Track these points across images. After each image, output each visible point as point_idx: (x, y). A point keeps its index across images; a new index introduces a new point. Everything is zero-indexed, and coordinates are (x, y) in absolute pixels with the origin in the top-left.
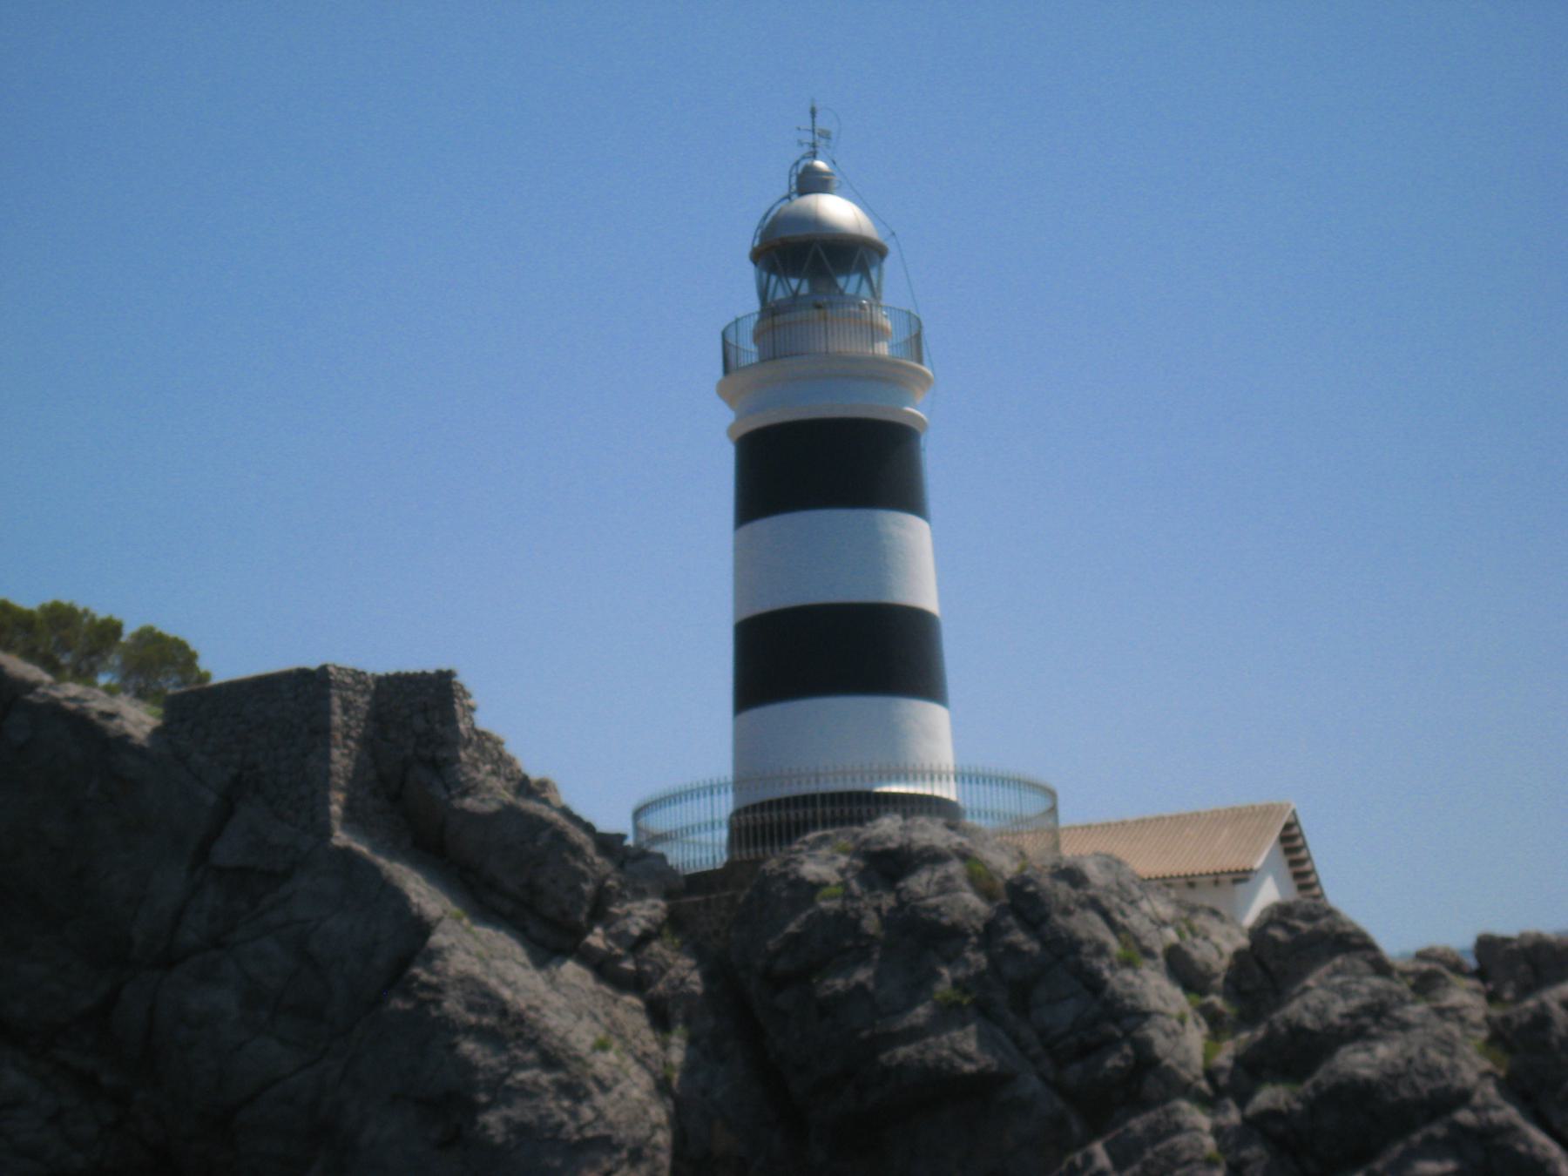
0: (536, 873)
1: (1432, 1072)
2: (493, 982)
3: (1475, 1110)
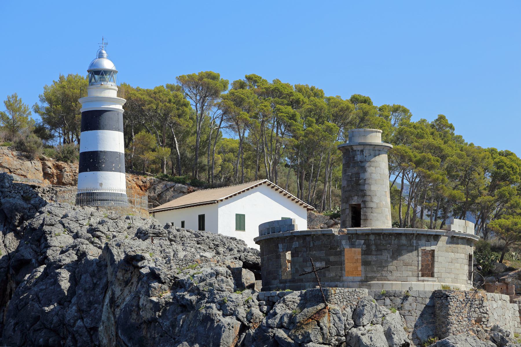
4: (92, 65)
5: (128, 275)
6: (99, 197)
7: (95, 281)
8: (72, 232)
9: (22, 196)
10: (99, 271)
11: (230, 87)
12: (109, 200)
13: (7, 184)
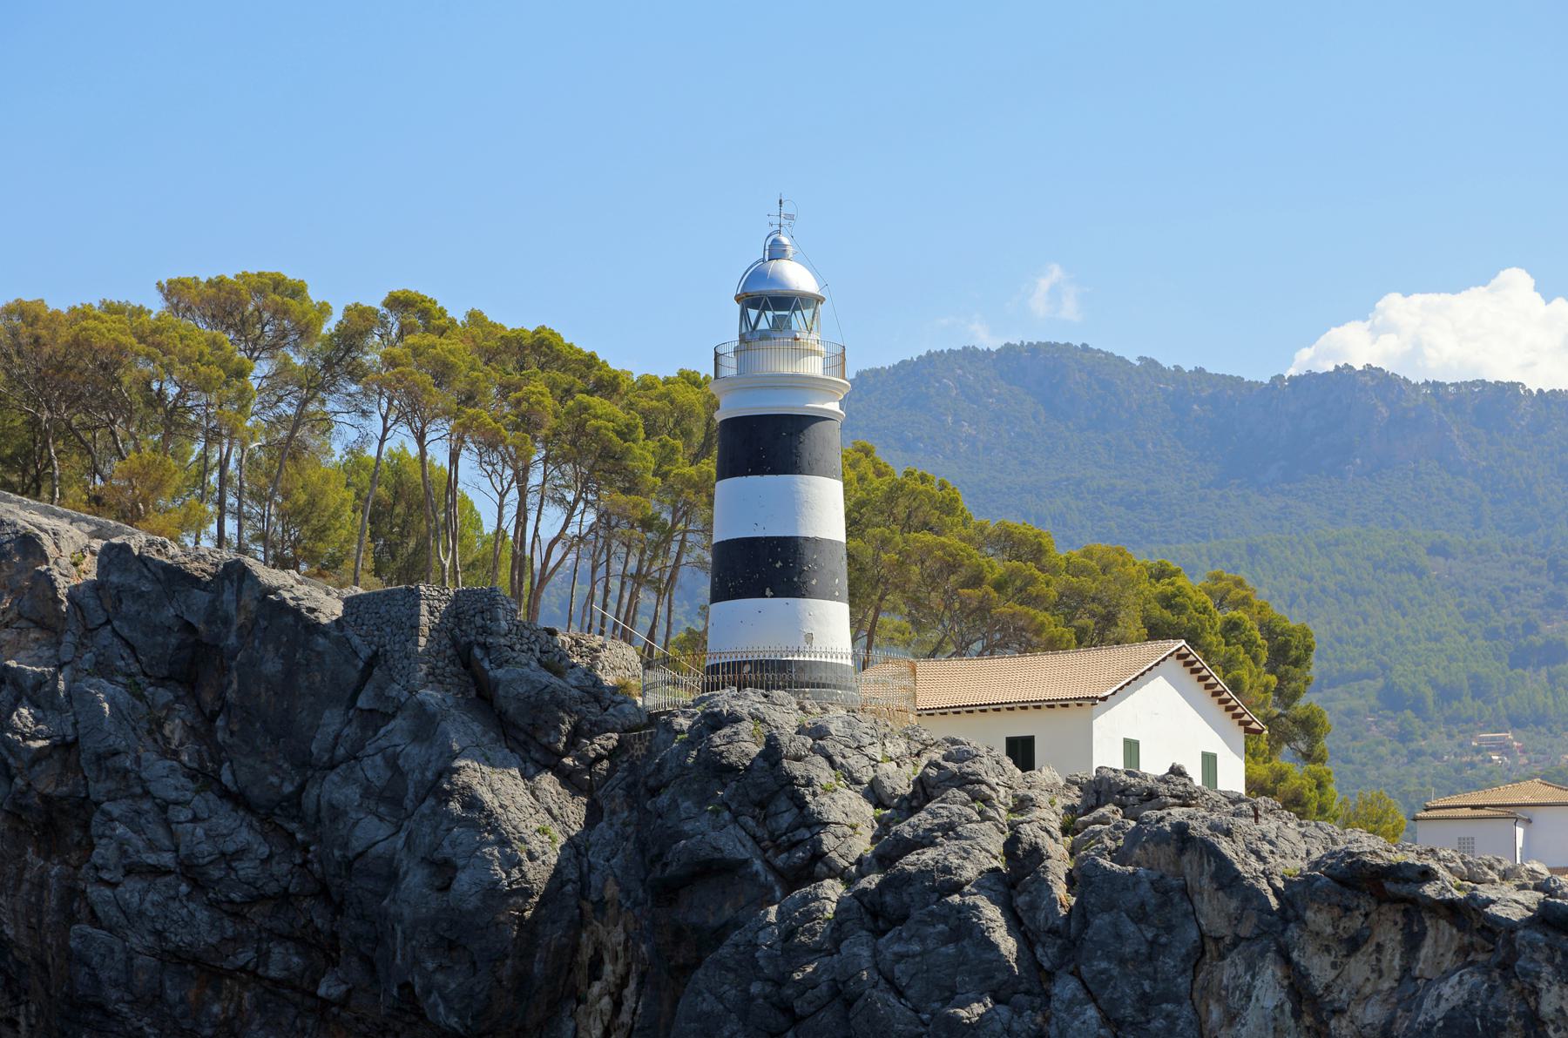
1: (947, 870)
4: (757, 275)
5: (1355, 922)
6: (805, 678)
7: (1149, 936)
8: (859, 783)
9: (539, 660)
10: (1162, 906)
11: (153, 316)
12: (829, 686)
13: (503, 623)
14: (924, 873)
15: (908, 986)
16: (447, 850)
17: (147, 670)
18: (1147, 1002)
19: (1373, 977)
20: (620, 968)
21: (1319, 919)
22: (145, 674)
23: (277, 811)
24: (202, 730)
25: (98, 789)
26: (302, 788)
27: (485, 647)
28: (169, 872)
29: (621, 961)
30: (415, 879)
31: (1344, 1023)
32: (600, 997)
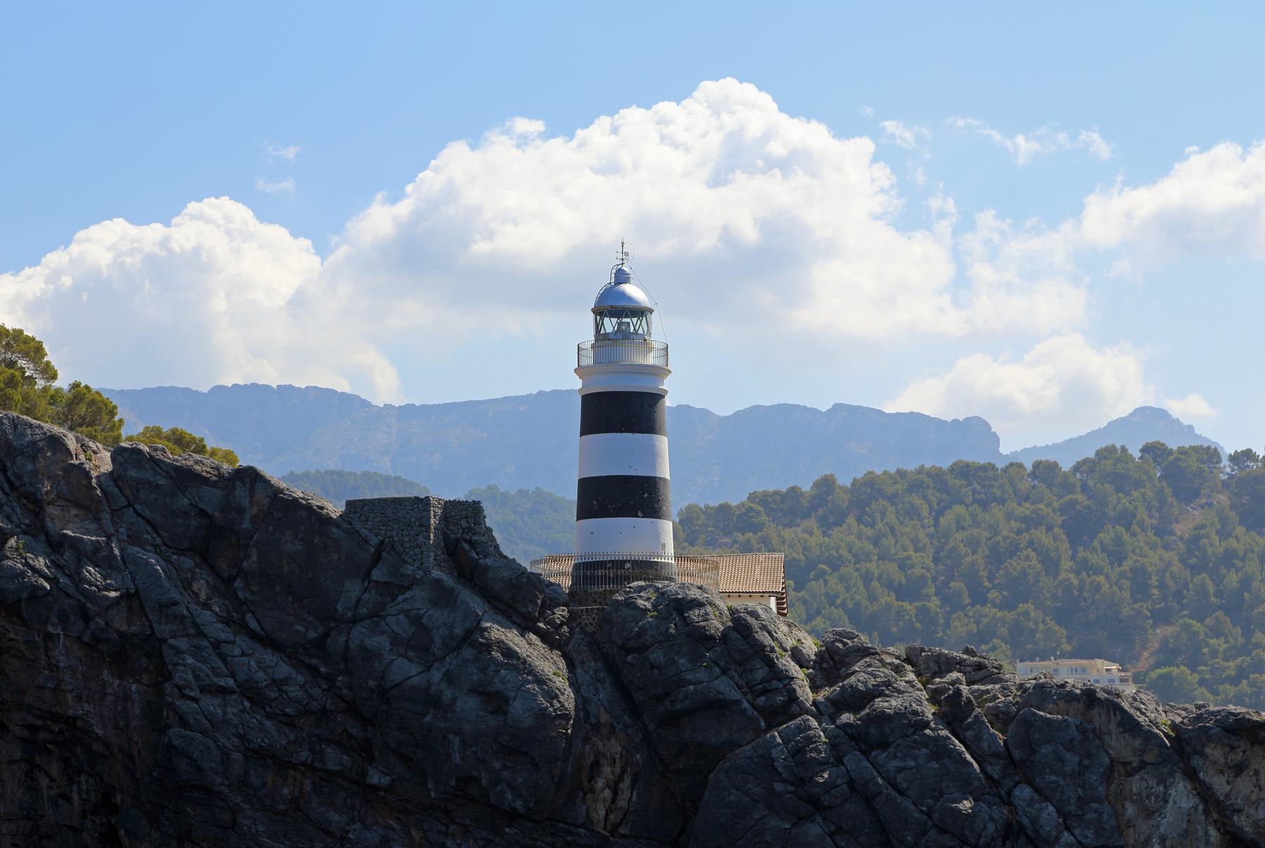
0: (520, 597)
1: (915, 713)
2: (511, 644)
3: (932, 730)
14: (899, 715)
15: (908, 788)
16: (498, 686)
17: (169, 543)
18: (1081, 802)
19: (1256, 790)
20: (618, 770)
21: (1215, 753)
22: (165, 545)
23: (301, 650)
24: (224, 585)
25: (164, 629)
26: (326, 635)
27: (470, 542)
28: (233, 692)
29: (618, 765)
30: (468, 705)
31: (1243, 818)
32: (603, 790)
